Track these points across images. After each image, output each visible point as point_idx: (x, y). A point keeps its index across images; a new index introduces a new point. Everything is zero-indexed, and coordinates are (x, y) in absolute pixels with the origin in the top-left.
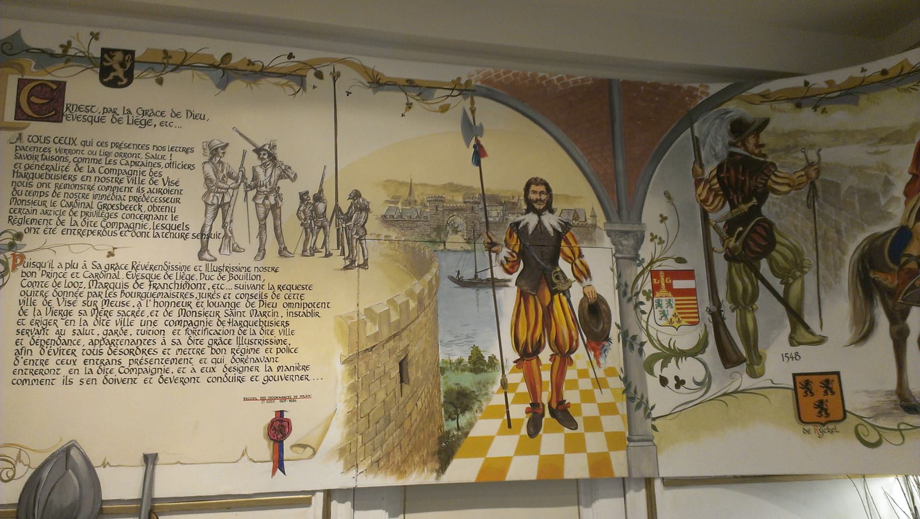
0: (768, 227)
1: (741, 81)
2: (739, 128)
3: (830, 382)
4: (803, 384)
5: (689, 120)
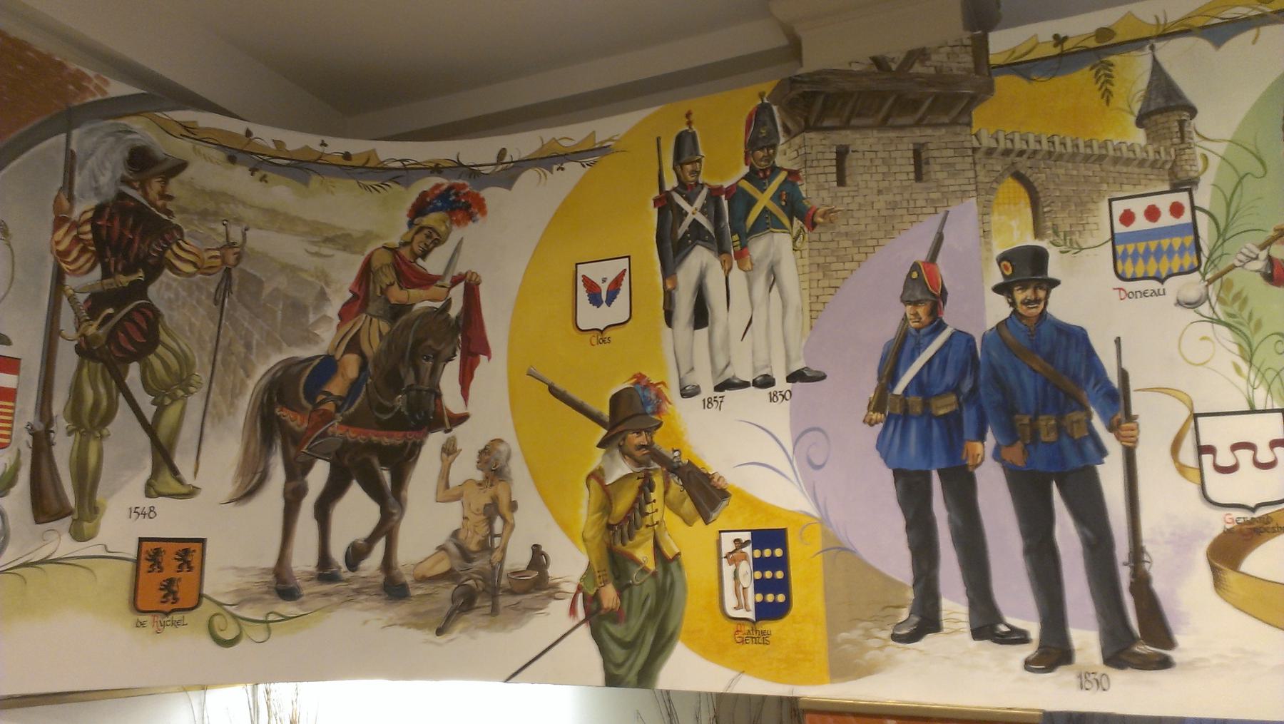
0: (152, 318)
1: (160, 94)
2: (141, 161)
3: (189, 553)
4: (151, 553)
5: (68, 119)
